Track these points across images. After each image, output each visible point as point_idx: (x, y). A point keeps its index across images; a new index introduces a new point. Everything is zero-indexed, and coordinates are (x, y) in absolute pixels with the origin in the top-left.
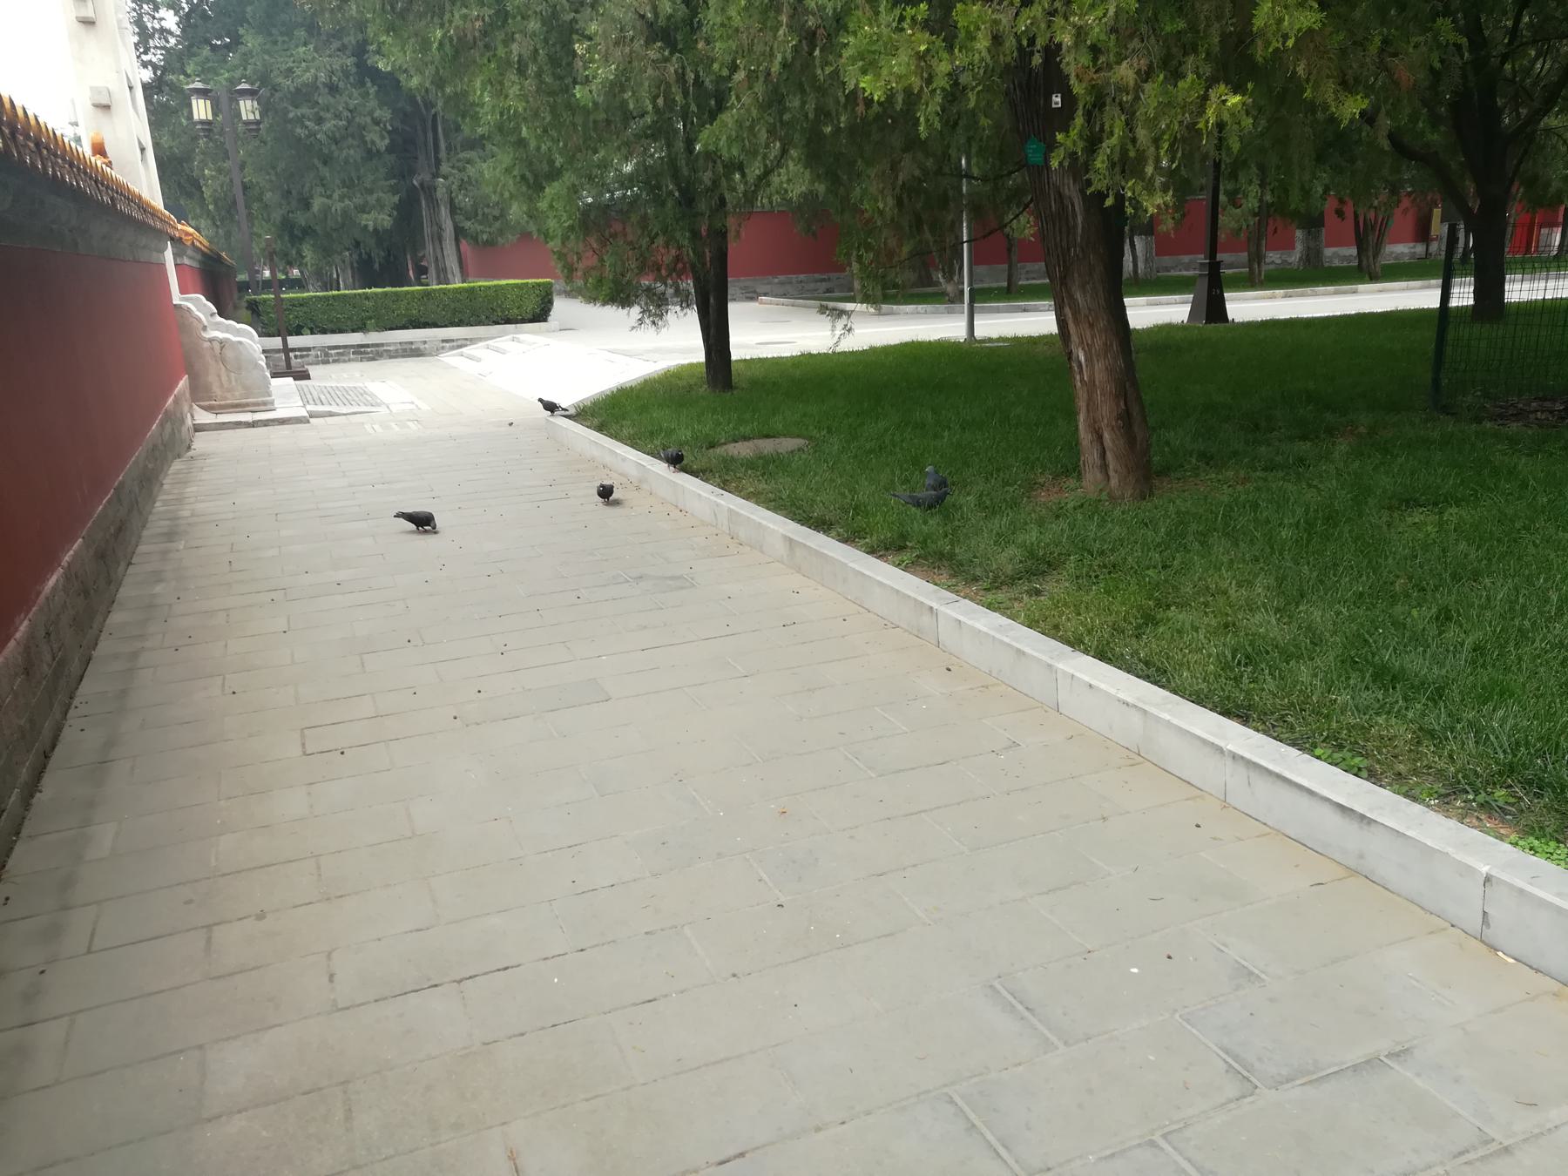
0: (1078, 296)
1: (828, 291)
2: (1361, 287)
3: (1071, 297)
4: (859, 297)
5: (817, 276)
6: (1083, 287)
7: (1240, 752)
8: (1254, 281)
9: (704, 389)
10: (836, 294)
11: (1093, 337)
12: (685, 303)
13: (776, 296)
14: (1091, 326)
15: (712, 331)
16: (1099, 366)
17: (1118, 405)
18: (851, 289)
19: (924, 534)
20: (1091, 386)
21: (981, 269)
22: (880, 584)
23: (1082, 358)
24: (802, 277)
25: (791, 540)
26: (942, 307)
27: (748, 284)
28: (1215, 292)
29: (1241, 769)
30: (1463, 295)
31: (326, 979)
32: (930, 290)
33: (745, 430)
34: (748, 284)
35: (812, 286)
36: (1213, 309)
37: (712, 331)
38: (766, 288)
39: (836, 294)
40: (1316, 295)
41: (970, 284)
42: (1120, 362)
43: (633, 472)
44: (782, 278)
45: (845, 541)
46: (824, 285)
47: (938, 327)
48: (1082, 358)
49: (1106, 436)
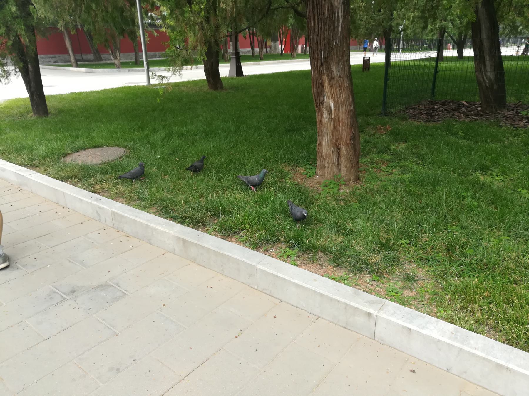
0: (334, 69)
1: (55, 62)
3: (330, 70)
4: (74, 65)
5: (49, 55)
6: (338, 64)
7: (326, 293)
8: (253, 58)
9: (32, 116)
10: (59, 64)
11: (340, 93)
12: (225, 78)
14: (340, 87)
15: (32, 84)
16: (342, 110)
17: (351, 131)
18: (70, 61)
19: (127, 181)
20: (335, 122)
21: (149, 53)
22: (297, 286)
23: (332, 105)
25: (184, 241)
26: (115, 70)
30: (225, 70)
32: (102, 62)
33: (80, 143)
35: (48, 60)
36: (239, 71)
37: (32, 84)
39: (59, 64)
40: (248, 65)
41: (147, 60)
42: (352, 108)
43: (13, 178)
45: (256, 246)
46: (53, 60)
47: (135, 78)
48: (332, 105)
49: (343, 149)
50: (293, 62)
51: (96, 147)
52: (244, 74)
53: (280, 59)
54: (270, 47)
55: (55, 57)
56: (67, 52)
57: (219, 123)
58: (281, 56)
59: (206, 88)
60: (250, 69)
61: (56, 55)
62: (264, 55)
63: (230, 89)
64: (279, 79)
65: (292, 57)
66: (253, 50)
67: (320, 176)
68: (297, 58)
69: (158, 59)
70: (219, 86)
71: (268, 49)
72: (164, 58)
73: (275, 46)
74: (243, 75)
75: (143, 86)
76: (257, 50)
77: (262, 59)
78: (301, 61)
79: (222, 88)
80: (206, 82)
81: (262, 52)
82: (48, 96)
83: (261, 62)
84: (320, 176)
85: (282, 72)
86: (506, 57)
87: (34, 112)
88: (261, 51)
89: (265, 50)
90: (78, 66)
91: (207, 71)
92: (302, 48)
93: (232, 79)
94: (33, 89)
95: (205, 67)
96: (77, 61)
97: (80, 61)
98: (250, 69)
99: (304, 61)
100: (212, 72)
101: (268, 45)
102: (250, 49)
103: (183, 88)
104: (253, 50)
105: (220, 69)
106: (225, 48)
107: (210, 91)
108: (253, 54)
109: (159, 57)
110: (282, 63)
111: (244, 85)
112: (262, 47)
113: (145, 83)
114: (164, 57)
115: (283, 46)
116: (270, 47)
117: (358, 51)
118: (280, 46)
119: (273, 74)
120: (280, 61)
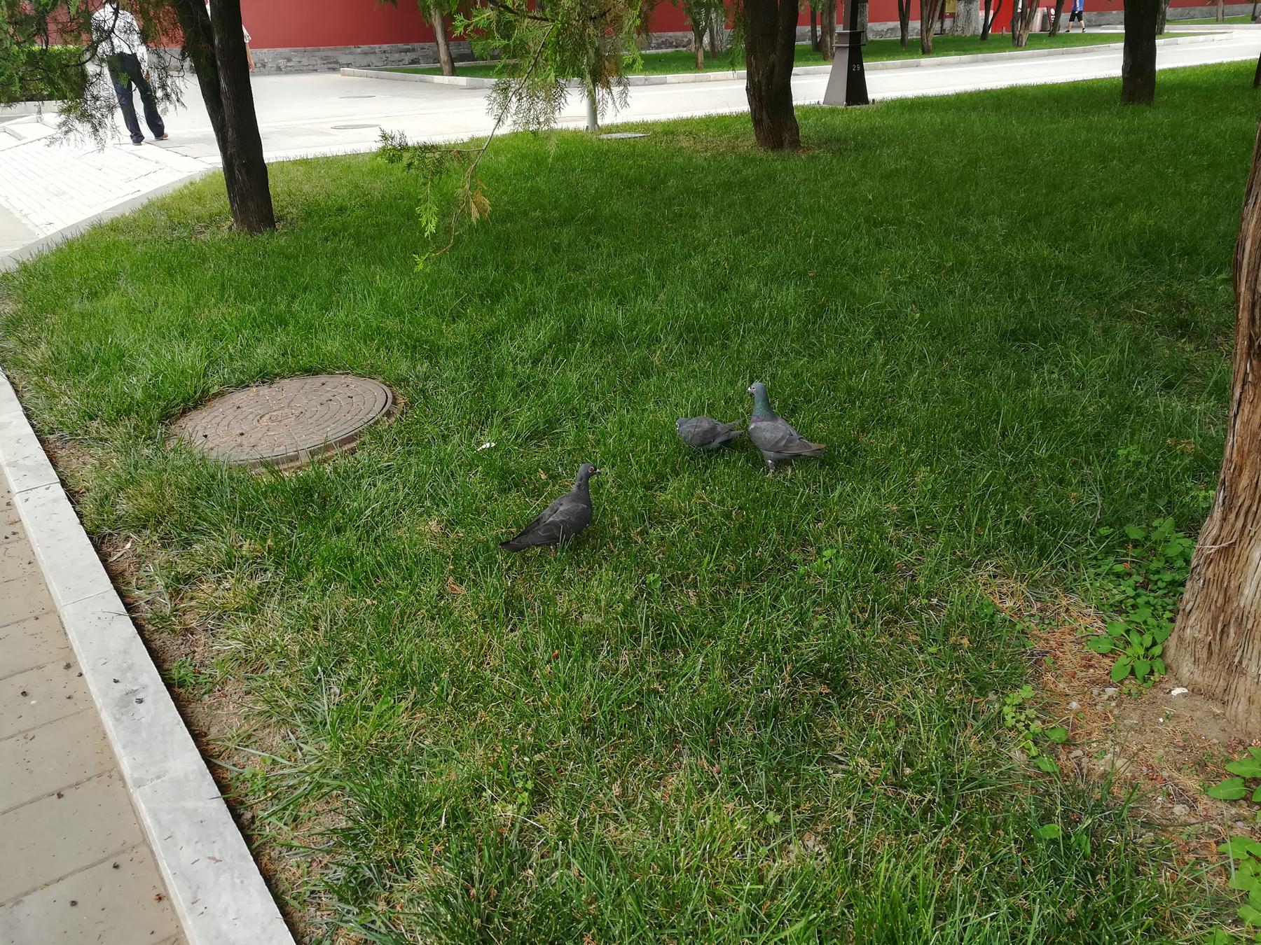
1: (413, 62)
2: (670, 77)
4: (446, 68)
5: (401, 46)
8: (903, 48)
10: (423, 66)
12: (810, 110)
13: (360, 67)
18: (437, 60)
24: (385, 47)
27: (330, 54)
28: (856, 68)
29: (199, 711)
30: (811, 86)
31: (55, 787)
34: (330, 54)
35: (396, 56)
36: (856, 90)
38: (350, 59)
39: (423, 66)
44: (365, 48)
46: (408, 57)
50: (1017, 58)
51: (310, 371)
52: (870, 97)
53: (979, 50)
54: (952, 16)
55: (413, 50)
56: (434, 40)
57: (752, 287)
58: (981, 43)
59: (749, 141)
60: (888, 82)
61: (416, 45)
62: (933, 41)
63: (819, 147)
64: (974, 116)
65: (1016, 43)
66: (904, 26)
67: (1195, 691)
68: (1029, 46)
69: (653, 51)
70: (786, 136)
71: (948, 23)
72: (670, 50)
73: (968, 12)
74: (866, 101)
75: (576, 132)
76: (915, 25)
77: (926, 52)
78: (1040, 56)
79: (796, 144)
80: (750, 125)
81: (928, 30)
82: (281, 165)
83: (924, 61)
84: (1195, 691)
85: (986, 91)
86: (717, 59)
87: (235, 216)
88: (926, 29)
89: (937, 26)
90: (454, 72)
91: (754, 92)
92: (1046, 17)
93: (832, 111)
94: (231, 150)
95: (750, 77)
96: (452, 60)
97: (462, 58)
98: (888, 82)
99: (1050, 55)
100: (770, 96)
101: (948, 10)
102: (898, 24)
103: (685, 143)
104: (904, 26)
105: (795, 82)
106: (826, 22)
107: (760, 153)
108: (903, 36)
109: (659, 47)
110: (986, 61)
111: (868, 134)
112: (931, 16)
113: (583, 124)
114: (671, 46)
115: (992, 12)
116: (952, 16)
117: (1217, 21)
118: (982, 14)
119: (958, 96)
120: (980, 56)
